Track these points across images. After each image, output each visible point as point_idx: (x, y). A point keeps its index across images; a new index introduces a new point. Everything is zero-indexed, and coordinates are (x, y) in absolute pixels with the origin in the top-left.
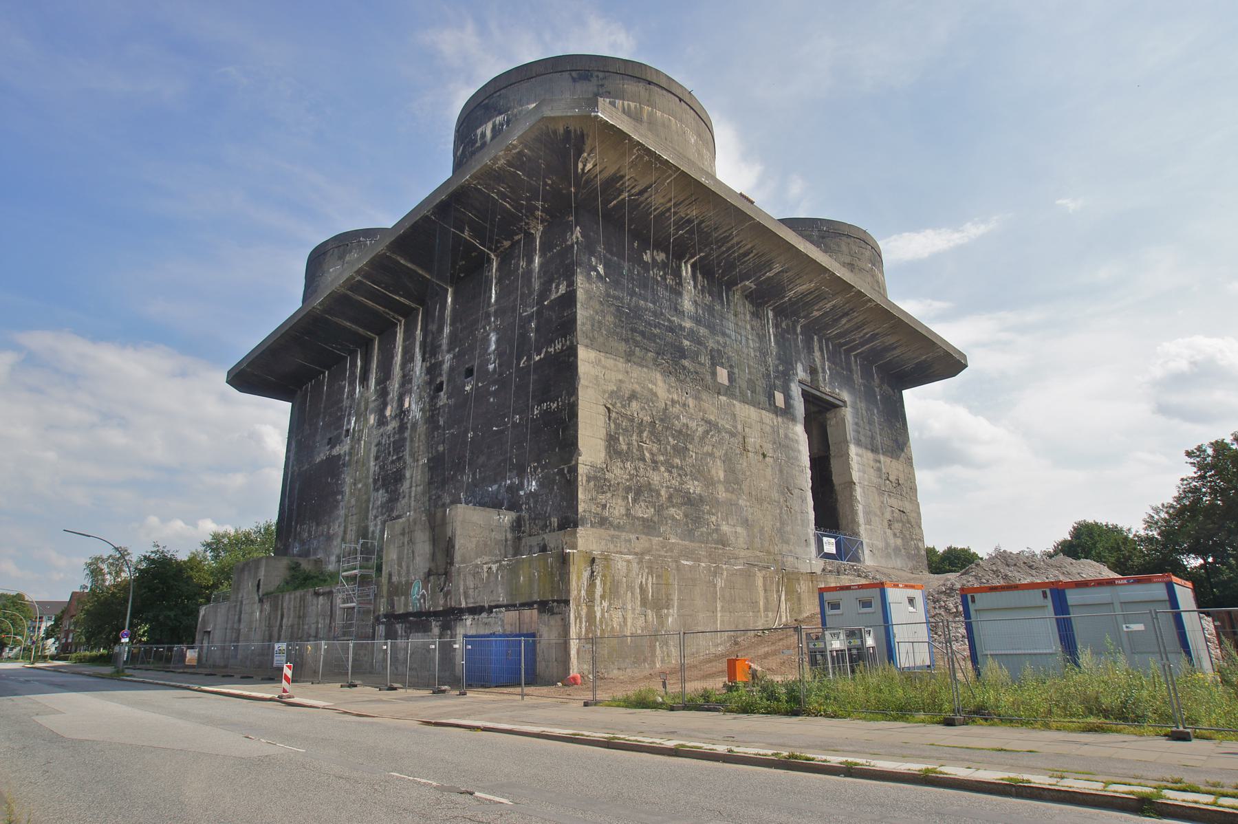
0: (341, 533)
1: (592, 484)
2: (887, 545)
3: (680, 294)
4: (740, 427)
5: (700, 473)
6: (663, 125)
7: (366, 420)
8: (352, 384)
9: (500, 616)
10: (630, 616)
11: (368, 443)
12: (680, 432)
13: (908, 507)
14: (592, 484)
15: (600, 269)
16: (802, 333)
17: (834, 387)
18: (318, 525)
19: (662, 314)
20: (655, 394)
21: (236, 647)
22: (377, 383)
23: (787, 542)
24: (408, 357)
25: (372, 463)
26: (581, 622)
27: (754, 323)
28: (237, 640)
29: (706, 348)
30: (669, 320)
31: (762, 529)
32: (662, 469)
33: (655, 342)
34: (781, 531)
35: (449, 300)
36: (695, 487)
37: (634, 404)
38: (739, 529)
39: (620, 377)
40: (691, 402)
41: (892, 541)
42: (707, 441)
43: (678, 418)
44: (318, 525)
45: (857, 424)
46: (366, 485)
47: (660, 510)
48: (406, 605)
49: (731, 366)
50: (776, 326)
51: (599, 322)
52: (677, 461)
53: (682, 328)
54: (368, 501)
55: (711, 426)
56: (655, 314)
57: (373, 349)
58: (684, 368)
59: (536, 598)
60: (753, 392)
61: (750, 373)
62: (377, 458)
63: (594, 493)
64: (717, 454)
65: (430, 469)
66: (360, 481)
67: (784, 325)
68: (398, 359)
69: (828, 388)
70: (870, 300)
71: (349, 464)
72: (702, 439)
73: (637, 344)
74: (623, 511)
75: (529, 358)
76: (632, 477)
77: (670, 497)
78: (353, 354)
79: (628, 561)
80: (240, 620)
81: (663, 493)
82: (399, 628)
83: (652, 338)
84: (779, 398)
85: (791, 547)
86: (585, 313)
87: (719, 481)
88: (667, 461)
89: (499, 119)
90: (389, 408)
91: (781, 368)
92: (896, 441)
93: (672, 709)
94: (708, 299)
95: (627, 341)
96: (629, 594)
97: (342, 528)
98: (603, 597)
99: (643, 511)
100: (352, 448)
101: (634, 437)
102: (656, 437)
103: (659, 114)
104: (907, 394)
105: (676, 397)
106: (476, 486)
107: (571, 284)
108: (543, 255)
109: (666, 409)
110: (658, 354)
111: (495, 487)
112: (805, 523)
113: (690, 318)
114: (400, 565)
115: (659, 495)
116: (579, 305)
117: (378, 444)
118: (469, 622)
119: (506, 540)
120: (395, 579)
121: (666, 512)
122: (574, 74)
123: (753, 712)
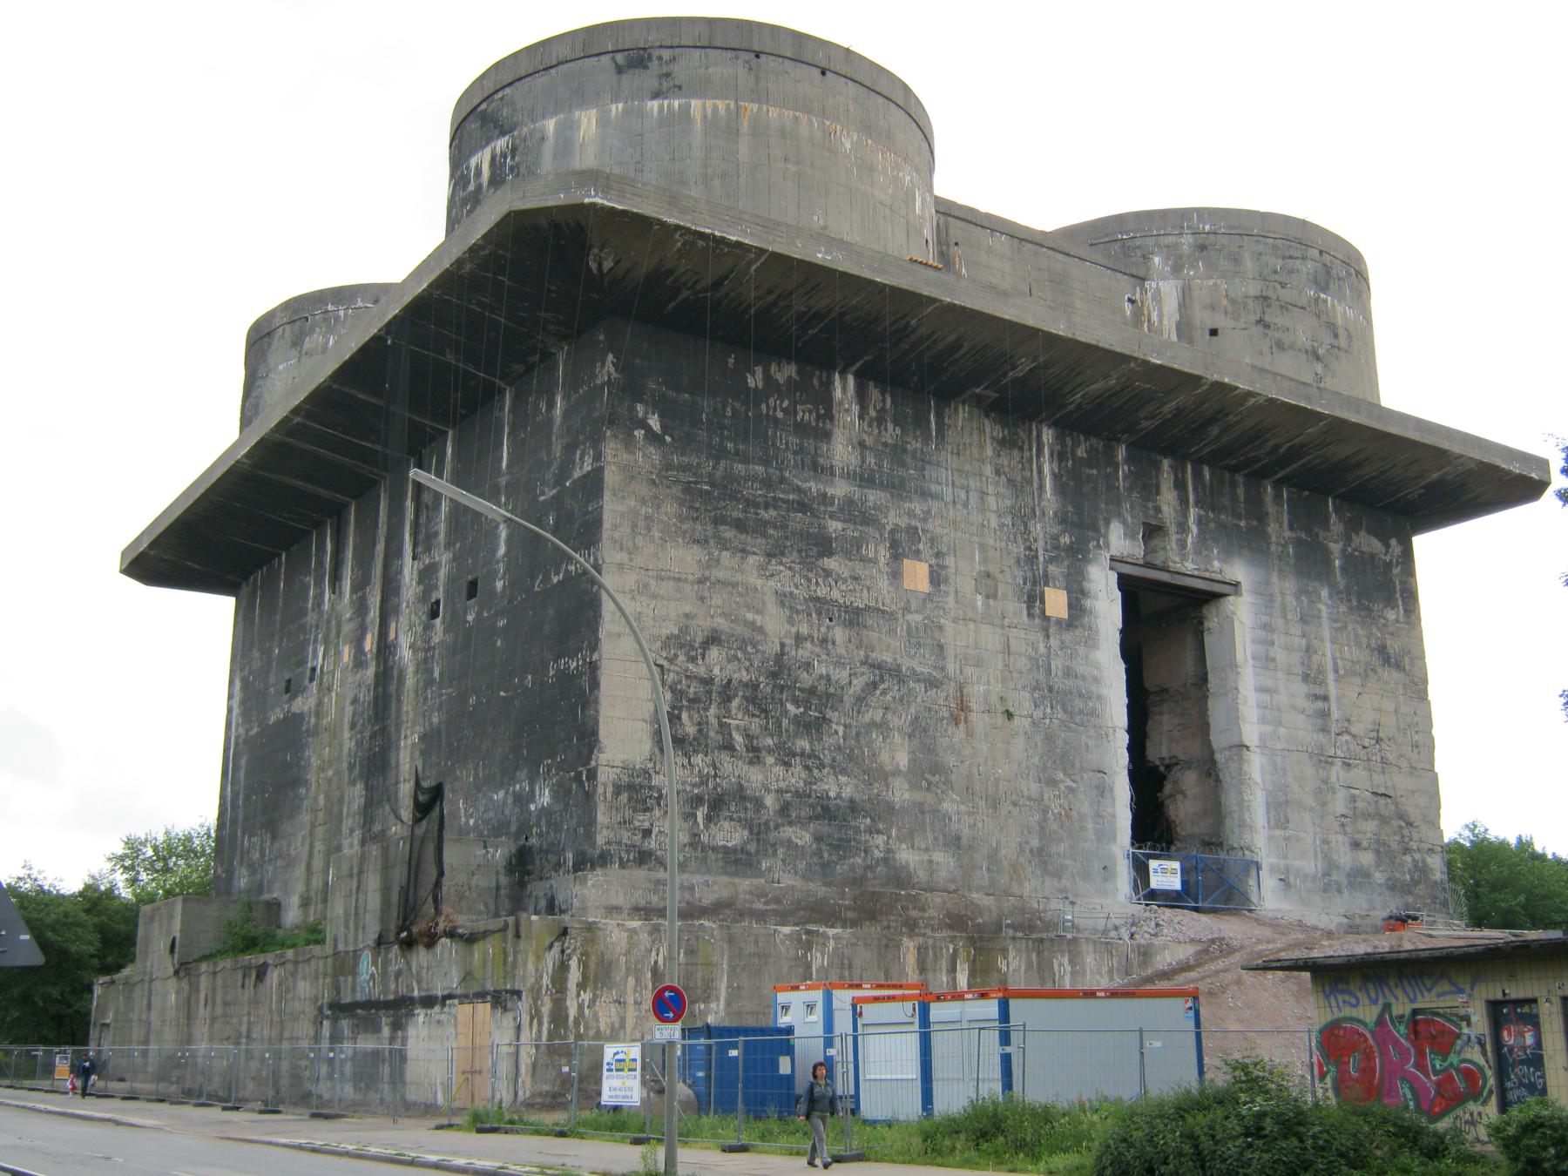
0: (305, 856)
1: (624, 797)
2: (1331, 866)
3: (827, 436)
4: (951, 668)
5: (851, 760)
6: (782, 133)
7: (338, 654)
8: (319, 583)
9: (453, 1010)
10: (631, 1014)
11: (341, 697)
12: (812, 691)
13: (1399, 782)
14: (624, 797)
15: (654, 422)
16: (1128, 461)
17: (1209, 559)
18: (274, 838)
19: (782, 480)
20: (761, 630)
21: (145, 1054)
22: (354, 590)
23: (1057, 875)
24: (393, 553)
25: (347, 735)
26: (540, 1024)
27: (1004, 461)
28: (146, 1042)
29: (881, 528)
30: (799, 490)
31: (993, 857)
32: (770, 760)
33: (764, 535)
34: (1041, 855)
35: (449, 451)
36: (840, 788)
37: (714, 653)
38: (938, 856)
39: (687, 609)
40: (839, 634)
41: (1345, 857)
42: (873, 701)
43: (808, 666)
44: (274, 838)
45: (1266, 627)
46: (338, 773)
47: (758, 831)
48: (354, 991)
49: (938, 555)
50: (1061, 456)
51: (648, 518)
52: (803, 744)
53: (825, 499)
54: (341, 801)
55: (883, 673)
56: (767, 483)
57: (347, 523)
58: (827, 573)
59: (490, 987)
60: (991, 595)
61: (985, 561)
62: (353, 726)
63: (628, 813)
64: (895, 721)
65: (424, 753)
66: (330, 763)
67: (1081, 452)
68: (380, 548)
69: (1187, 562)
70: (1250, 394)
71: (315, 732)
72: (860, 700)
73: (724, 545)
74: (684, 838)
75: (547, 579)
76: (704, 780)
77: (784, 809)
78: (319, 525)
79: (633, 931)
80: (149, 1006)
81: (769, 801)
82: (345, 1024)
83: (761, 528)
84: (1056, 602)
85: (1065, 882)
86: (620, 508)
87: (896, 772)
88: (779, 746)
89: (501, 144)
90: (369, 636)
91: (1066, 539)
92: (1382, 650)
93: (562, 1134)
94: (891, 433)
95: (702, 542)
96: (631, 980)
97: (307, 847)
98: (582, 986)
99: (729, 834)
100: (320, 704)
101: (713, 711)
102: (755, 701)
103: (773, 113)
104: (1427, 546)
105: (804, 630)
106: (479, 790)
107: (598, 457)
108: (566, 398)
109: (782, 654)
110: (770, 555)
111: (501, 794)
112: (1105, 835)
113: (848, 476)
114: (347, 926)
115: (759, 804)
116: (607, 496)
117: (355, 701)
118: (421, 1019)
119: (498, 888)
120: (341, 947)
121: (773, 836)
122: (620, 58)
123: (868, 1160)
